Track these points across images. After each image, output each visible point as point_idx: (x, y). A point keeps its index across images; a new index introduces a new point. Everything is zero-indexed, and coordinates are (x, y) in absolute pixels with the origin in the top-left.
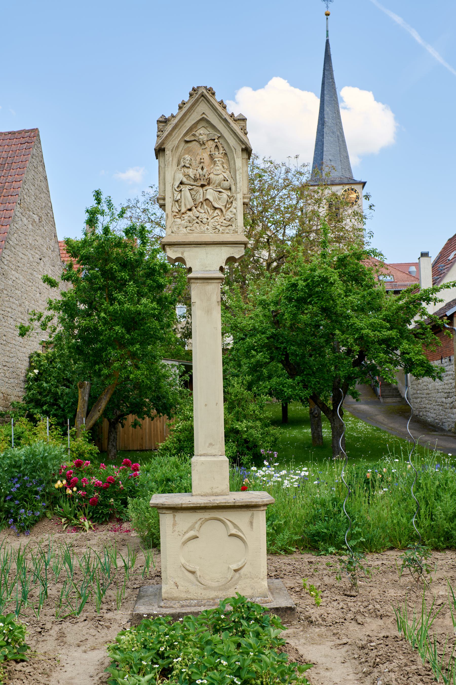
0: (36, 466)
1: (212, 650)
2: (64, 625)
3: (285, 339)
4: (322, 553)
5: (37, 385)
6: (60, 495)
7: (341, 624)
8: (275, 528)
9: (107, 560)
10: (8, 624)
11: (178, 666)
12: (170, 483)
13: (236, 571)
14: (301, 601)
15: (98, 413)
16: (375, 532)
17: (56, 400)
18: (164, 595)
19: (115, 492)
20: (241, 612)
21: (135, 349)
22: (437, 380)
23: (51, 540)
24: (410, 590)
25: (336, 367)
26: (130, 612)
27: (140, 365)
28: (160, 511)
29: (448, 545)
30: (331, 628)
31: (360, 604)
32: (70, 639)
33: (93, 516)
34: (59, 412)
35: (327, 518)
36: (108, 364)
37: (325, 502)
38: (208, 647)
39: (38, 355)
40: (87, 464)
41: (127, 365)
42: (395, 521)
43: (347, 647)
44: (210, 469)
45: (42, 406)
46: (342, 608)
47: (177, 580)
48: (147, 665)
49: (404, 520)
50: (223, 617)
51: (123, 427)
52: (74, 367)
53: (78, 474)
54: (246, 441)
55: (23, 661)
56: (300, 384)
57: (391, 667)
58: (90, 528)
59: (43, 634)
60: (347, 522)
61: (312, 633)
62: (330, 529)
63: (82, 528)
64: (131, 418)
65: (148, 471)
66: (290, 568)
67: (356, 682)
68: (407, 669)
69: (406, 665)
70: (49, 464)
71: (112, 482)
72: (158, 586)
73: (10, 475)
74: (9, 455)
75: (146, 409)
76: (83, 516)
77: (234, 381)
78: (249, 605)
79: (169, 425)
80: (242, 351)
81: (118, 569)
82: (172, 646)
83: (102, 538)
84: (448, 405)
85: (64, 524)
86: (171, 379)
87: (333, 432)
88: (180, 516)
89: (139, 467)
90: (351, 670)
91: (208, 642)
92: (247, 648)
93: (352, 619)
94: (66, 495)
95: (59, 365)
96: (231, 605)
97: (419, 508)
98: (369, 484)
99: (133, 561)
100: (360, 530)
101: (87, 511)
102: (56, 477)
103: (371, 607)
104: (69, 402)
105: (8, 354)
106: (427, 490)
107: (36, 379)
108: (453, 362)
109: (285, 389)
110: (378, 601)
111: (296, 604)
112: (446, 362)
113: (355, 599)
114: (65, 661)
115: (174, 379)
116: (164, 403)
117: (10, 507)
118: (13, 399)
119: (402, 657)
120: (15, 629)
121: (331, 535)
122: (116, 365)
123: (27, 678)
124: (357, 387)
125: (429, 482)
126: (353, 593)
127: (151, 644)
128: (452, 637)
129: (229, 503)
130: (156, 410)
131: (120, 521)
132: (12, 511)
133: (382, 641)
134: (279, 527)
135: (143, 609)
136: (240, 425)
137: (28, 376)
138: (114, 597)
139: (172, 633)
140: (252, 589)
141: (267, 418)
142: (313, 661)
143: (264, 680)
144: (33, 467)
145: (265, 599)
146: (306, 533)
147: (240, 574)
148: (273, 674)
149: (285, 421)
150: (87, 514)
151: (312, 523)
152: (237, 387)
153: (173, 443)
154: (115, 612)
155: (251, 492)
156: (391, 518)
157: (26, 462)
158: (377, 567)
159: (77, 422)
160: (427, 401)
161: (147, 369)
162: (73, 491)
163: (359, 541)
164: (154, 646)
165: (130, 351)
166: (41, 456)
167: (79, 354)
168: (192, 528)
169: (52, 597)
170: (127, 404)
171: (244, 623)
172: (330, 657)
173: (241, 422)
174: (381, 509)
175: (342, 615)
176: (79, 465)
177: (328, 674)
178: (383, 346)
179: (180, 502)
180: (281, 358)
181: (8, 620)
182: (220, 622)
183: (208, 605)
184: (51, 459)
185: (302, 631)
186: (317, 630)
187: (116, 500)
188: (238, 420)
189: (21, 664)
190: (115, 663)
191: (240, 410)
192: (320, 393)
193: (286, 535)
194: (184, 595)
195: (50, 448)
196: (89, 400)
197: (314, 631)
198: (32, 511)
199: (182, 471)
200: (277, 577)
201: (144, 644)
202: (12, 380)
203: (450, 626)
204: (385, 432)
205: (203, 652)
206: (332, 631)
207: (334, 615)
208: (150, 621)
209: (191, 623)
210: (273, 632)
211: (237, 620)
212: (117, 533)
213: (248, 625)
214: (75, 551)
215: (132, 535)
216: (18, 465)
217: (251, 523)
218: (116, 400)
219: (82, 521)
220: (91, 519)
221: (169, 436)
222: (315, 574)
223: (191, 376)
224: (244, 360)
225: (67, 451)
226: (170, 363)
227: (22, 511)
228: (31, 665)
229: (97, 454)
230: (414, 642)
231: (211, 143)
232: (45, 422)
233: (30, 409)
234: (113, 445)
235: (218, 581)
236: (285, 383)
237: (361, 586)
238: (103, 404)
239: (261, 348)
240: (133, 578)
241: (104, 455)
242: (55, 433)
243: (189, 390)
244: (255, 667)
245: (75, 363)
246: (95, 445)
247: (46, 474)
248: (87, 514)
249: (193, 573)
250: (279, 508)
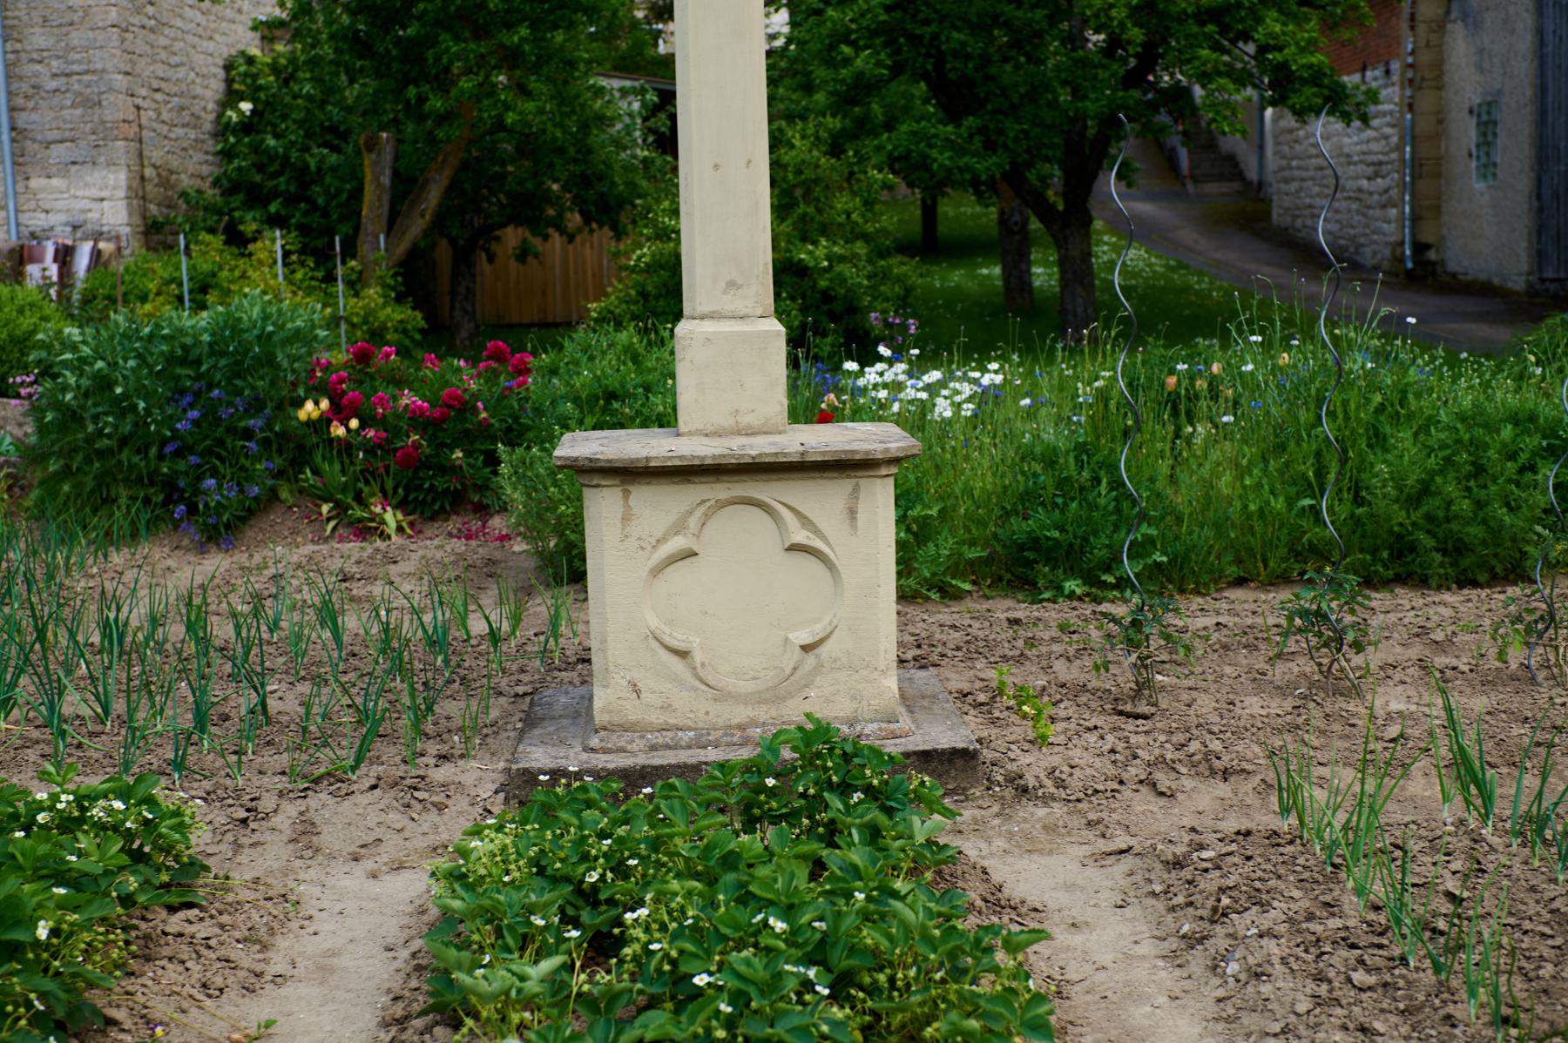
0: (246, 360)
1: (742, 885)
2: (313, 801)
3: (936, 11)
4: (1046, 595)
5: (250, 143)
6: (315, 440)
7: (1109, 794)
8: (915, 528)
9: (440, 617)
10: (139, 804)
11: (638, 932)
12: (616, 405)
13: (806, 648)
14: (994, 731)
15: (421, 221)
16: (1195, 536)
17: (304, 186)
18: (600, 718)
19: (466, 433)
20: (825, 769)
21: (516, 39)
22: (1357, 123)
23: (292, 561)
24: (1305, 698)
25: (1075, 93)
26: (502, 765)
27: (534, 83)
28: (585, 480)
29: (1400, 570)
30: (1080, 805)
31: (1162, 738)
32: (331, 838)
33: (406, 497)
34: (315, 220)
35: (1059, 501)
36: (443, 81)
37: (1057, 456)
38: (729, 878)
39: (251, 60)
40: (388, 355)
41: (495, 85)
42: (1252, 507)
43: (1128, 862)
44: (729, 359)
45: (266, 203)
46: (1113, 751)
47: (636, 675)
48: (546, 927)
49: (1279, 504)
50: (770, 782)
51: (491, 260)
52: (351, 94)
53: (361, 382)
54: (827, 296)
55: (190, 905)
56: (977, 139)
57: (1266, 922)
58: (400, 529)
59: (252, 825)
60: (1118, 510)
61: (1025, 820)
62: (1070, 529)
63: (376, 529)
64: (512, 236)
65: (554, 372)
66: (956, 637)
67: (1161, 963)
68: (1315, 927)
69: (1310, 917)
70: (280, 357)
71: (460, 406)
72: (583, 690)
73: (172, 384)
74: (166, 331)
75: (551, 212)
76: (378, 498)
77: (793, 134)
78: (849, 749)
79: (617, 255)
80: (814, 46)
81: (474, 642)
82: (622, 871)
83: (429, 555)
84: (1376, 197)
85: (329, 520)
86: (619, 126)
87: (1063, 272)
88: (644, 497)
89: (531, 361)
90: (1144, 928)
91: (730, 861)
92: (844, 880)
93: (1141, 782)
94: (331, 440)
95: (307, 88)
96: (794, 749)
97: (1321, 473)
98: (1180, 407)
99: (516, 620)
100: (1153, 532)
101: (389, 484)
102: (301, 392)
103: (1194, 746)
104: (339, 191)
105: (163, 55)
106: (1347, 418)
107: (247, 127)
108: (1395, 78)
109: (934, 153)
110: (1216, 729)
111: (979, 741)
112: (1375, 79)
113: (1148, 725)
114: (315, 902)
115: (627, 126)
116: (602, 195)
117: (176, 472)
118: (185, 182)
119: (1297, 894)
120: (162, 818)
121: (1071, 545)
122: (465, 84)
123: (200, 957)
124: (1125, 149)
125: (1354, 398)
126: (1144, 708)
127: (558, 865)
128: (1439, 833)
129: (785, 455)
130: (582, 213)
131: (483, 511)
132: (182, 484)
133: (1234, 847)
134: (924, 522)
135: (538, 756)
136: (810, 253)
137: (225, 120)
138: (457, 722)
139: (621, 831)
140: (853, 698)
141: (883, 231)
142: (1034, 899)
143: (900, 975)
144: (237, 363)
145: (892, 726)
146: (998, 540)
147: (817, 656)
148: (926, 959)
149: (930, 244)
150: (390, 492)
151: (1017, 513)
152: (799, 146)
153: (627, 302)
154: (461, 763)
155: (850, 425)
156: (1240, 497)
157: (215, 350)
158: (1203, 633)
159: (364, 247)
160: (1317, 189)
161: (553, 98)
162: (348, 430)
163: (1149, 561)
164: (568, 870)
165: (502, 46)
166: (256, 332)
167: (361, 57)
168: (678, 528)
169: (284, 719)
170: (502, 196)
171: (836, 803)
172: (1082, 889)
173: (815, 243)
174: (1212, 468)
175: (1111, 771)
176: (362, 357)
177: (1077, 939)
178: (1210, 28)
179: (643, 453)
180: (923, 66)
181: (141, 792)
182: (762, 797)
183: (728, 745)
184: (287, 341)
185: (997, 815)
186: (1041, 812)
187: (468, 454)
188: (804, 240)
189: (181, 915)
190: (447, 925)
191: (811, 210)
192: (1030, 165)
193: (944, 546)
194: (657, 718)
195: (279, 311)
196: (393, 186)
197: (1032, 814)
198: (238, 484)
199: (650, 370)
200: (921, 663)
201: (537, 865)
202: (180, 131)
203: (1423, 798)
204: (1200, 273)
205: (716, 893)
206: (1083, 814)
207: (1089, 771)
208: (556, 794)
209: (676, 803)
210: (922, 827)
211: (812, 791)
212: (473, 543)
213: (847, 805)
214: (355, 592)
215: (517, 548)
216: (192, 357)
217: (852, 513)
218: (467, 186)
219: (378, 509)
220: (401, 505)
221: (615, 282)
222: (1027, 652)
223: (673, 118)
224: (820, 73)
225: (338, 326)
226: (616, 83)
227: (211, 482)
228: (212, 917)
229: (421, 331)
230: (1330, 848)
232: (276, 242)
233: (232, 210)
234: (465, 310)
235: (755, 678)
236: (935, 136)
237: (1163, 688)
238: (433, 197)
239: (870, 38)
240: (514, 668)
241: (439, 335)
242: (299, 275)
243: (669, 159)
244: (869, 936)
245: (352, 81)
246: (414, 309)
247: (273, 383)
248: (390, 492)
249: (683, 654)
250: (925, 473)
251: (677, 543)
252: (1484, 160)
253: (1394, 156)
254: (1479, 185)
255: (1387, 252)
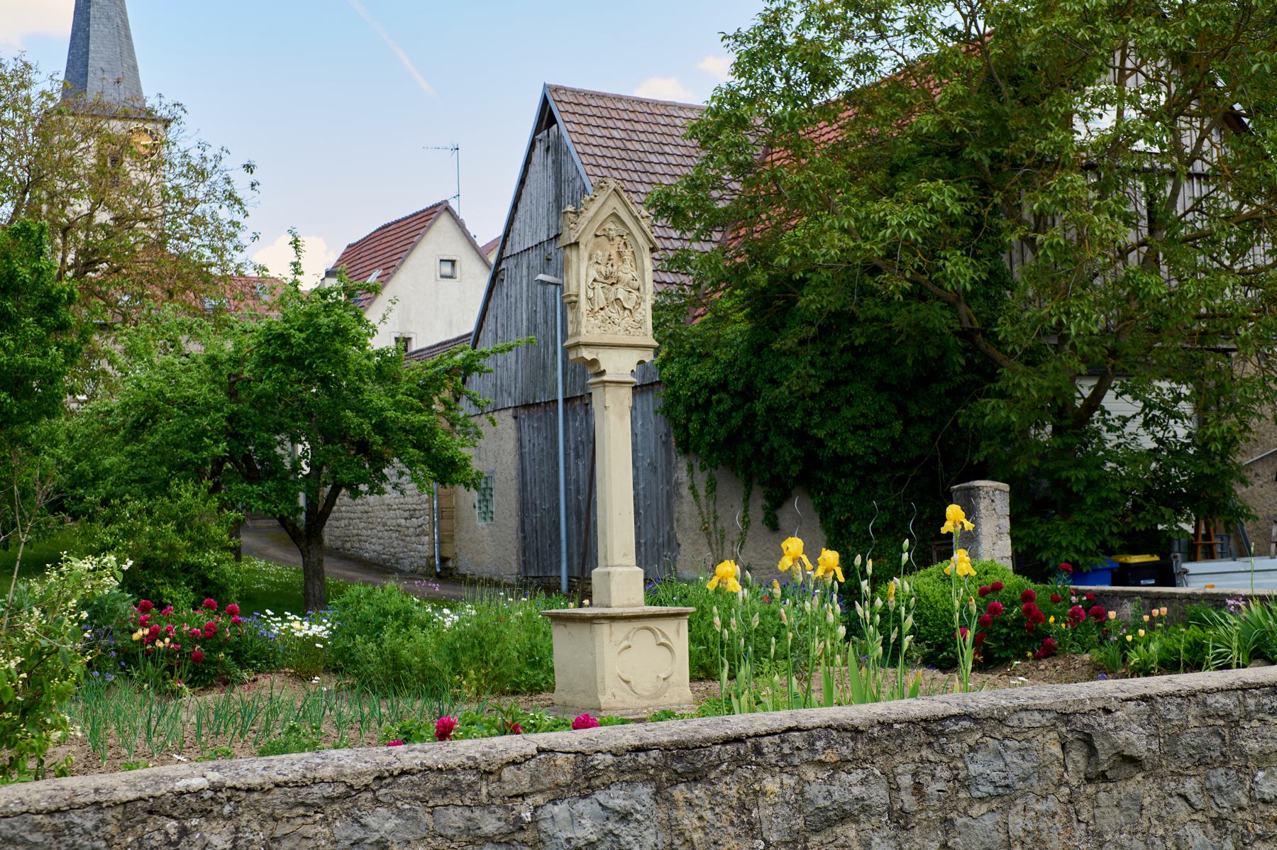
22: (472, 489)
168: (627, 638)
194: (620, 705)
217: (678, 631)
231: (618, 239)
249: (627, 682)
251: (625, 643)
252: (484, 509)
253: (426, 506)
254: (481, 524)
255: (423, 562)
